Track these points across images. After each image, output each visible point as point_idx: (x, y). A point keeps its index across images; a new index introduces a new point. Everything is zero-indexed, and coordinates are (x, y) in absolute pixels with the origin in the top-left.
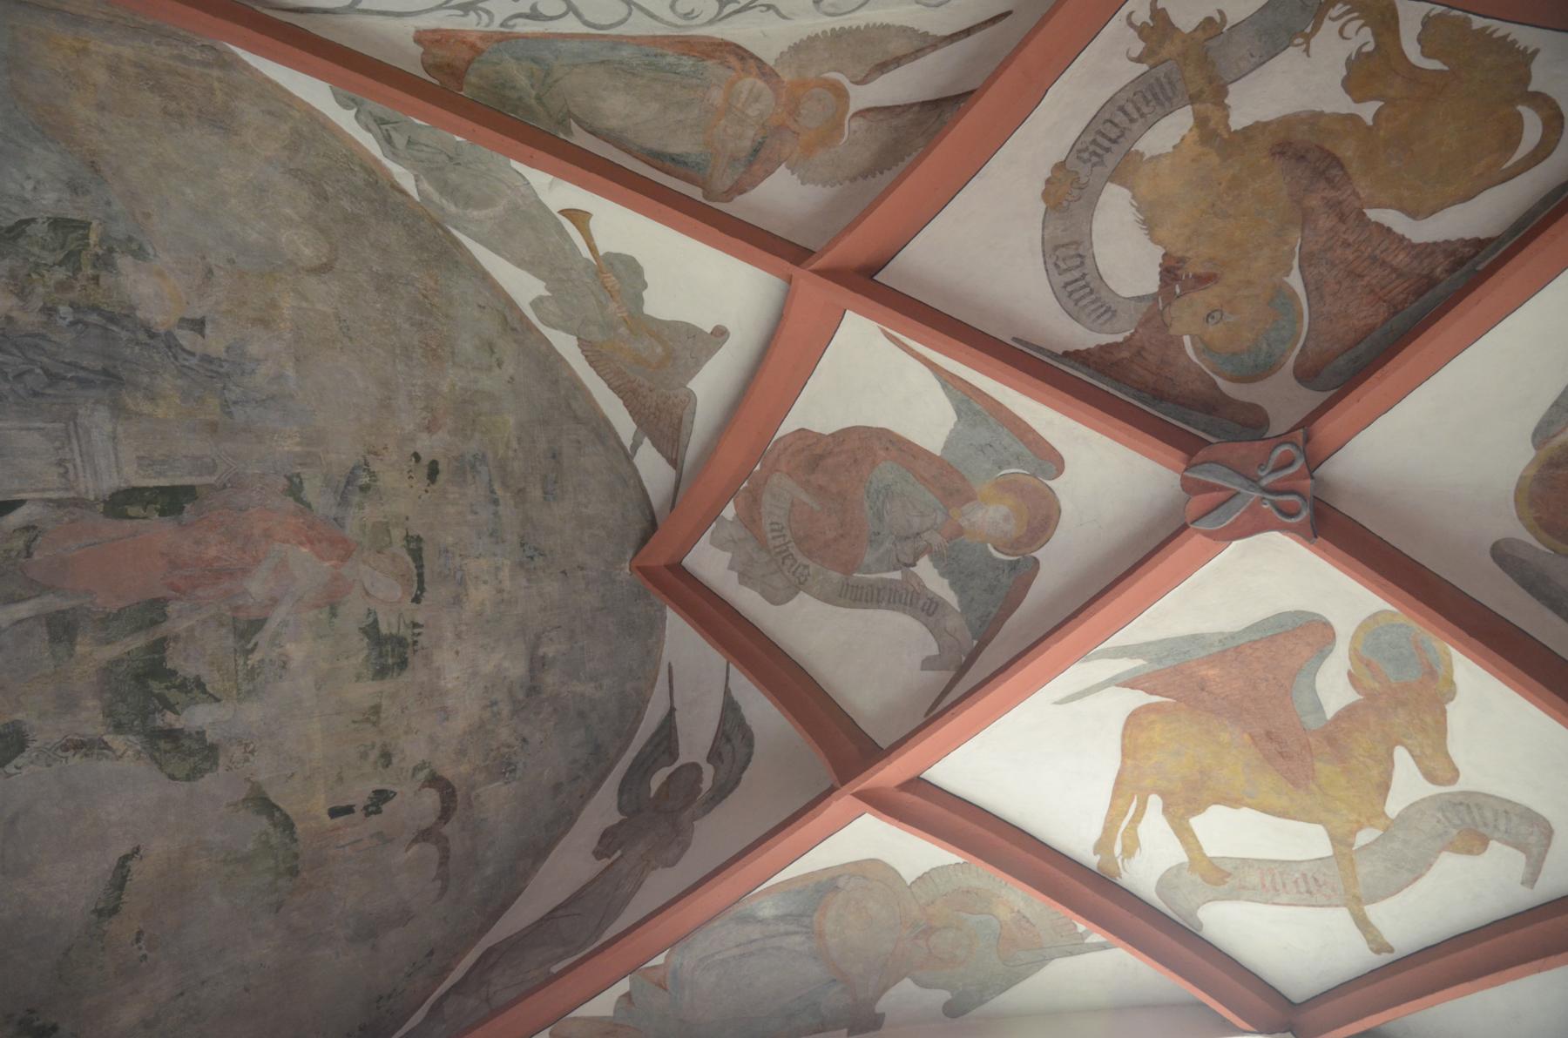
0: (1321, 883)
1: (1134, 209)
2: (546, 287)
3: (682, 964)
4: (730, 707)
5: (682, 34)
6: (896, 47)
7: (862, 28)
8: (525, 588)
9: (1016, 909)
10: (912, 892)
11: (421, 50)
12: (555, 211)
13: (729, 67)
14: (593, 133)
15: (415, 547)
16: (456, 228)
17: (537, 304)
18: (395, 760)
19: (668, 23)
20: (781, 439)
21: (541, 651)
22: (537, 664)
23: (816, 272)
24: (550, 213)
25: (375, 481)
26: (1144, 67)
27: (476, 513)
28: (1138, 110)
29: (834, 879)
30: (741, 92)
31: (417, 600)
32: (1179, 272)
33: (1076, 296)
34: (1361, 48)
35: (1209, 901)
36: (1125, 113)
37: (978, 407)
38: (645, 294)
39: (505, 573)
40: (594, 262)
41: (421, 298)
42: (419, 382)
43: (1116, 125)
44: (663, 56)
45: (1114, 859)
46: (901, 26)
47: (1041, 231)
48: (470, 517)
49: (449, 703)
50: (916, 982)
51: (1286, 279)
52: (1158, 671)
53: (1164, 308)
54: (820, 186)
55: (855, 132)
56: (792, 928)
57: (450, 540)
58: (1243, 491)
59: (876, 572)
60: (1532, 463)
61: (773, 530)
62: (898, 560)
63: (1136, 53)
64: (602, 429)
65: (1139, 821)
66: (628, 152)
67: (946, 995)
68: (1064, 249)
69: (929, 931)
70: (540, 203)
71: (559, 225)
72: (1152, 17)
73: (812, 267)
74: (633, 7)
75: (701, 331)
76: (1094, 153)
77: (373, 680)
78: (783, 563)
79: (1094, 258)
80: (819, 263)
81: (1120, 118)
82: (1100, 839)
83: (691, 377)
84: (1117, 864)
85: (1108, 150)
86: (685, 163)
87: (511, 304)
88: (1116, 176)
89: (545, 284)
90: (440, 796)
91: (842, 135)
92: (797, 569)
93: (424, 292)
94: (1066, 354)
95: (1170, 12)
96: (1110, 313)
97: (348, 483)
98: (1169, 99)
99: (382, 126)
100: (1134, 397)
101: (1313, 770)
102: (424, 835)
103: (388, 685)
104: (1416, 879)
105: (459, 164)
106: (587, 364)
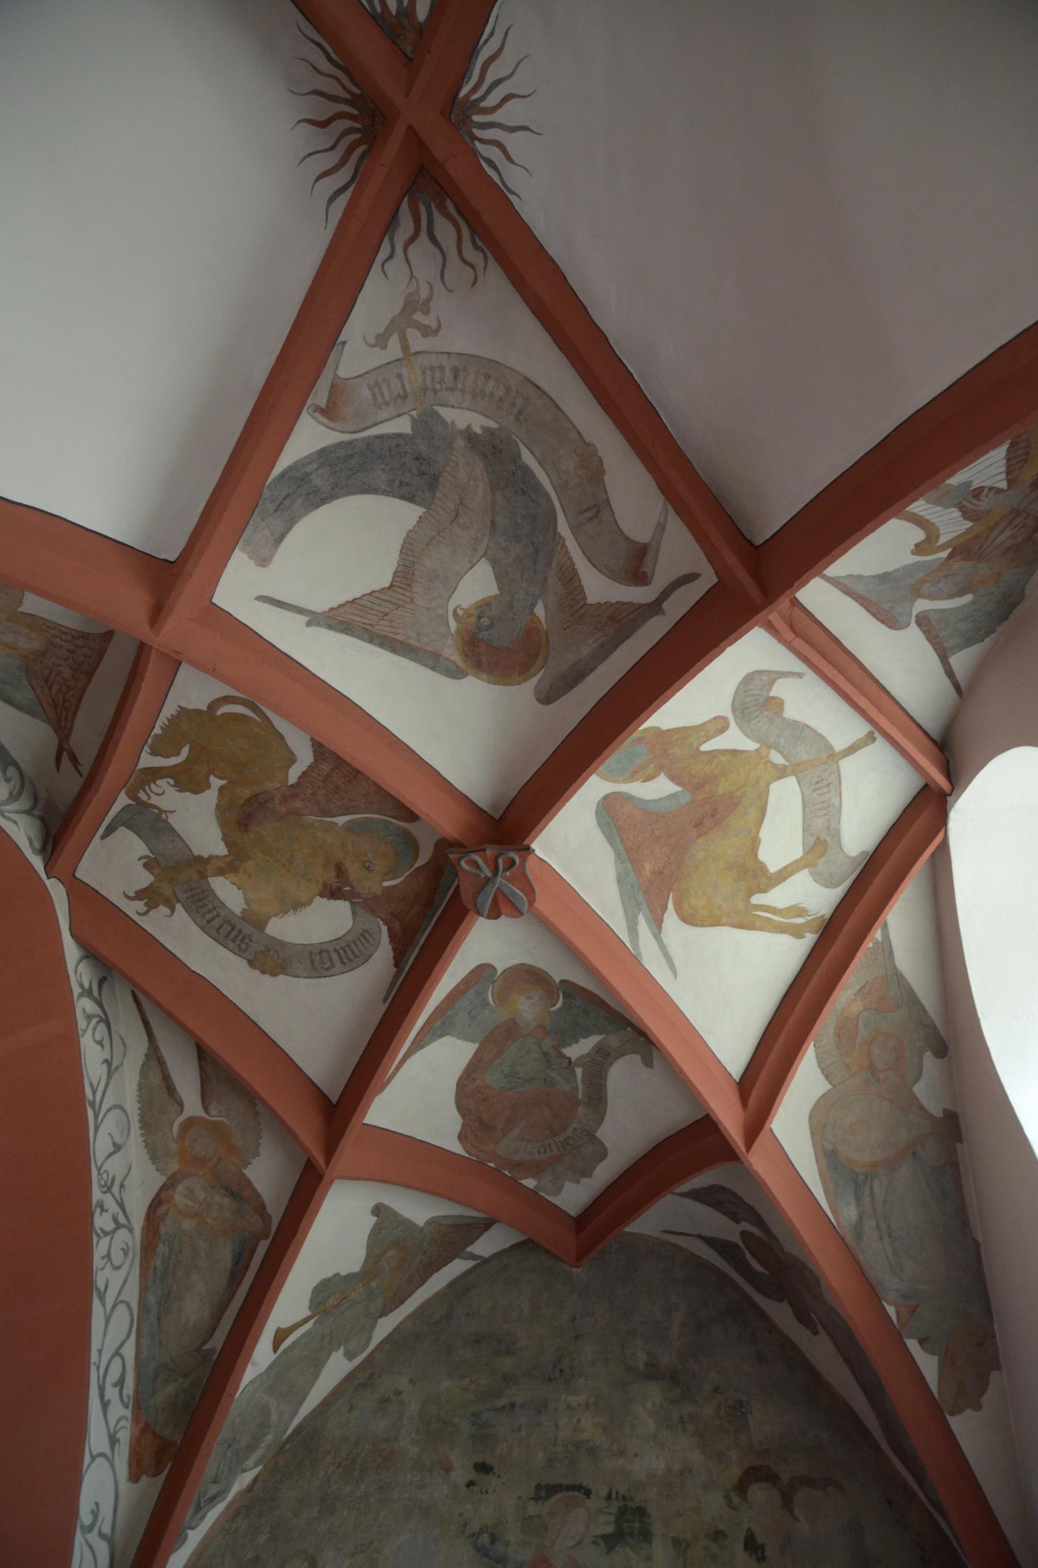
0: (820, 779)
1: (285, 916)
2: (336, 1351)
3: (897, 1291)
4: (694, 1195)
5: (139, 1252)
6: (156, 1078)
7: (140, 1106)
8: (586, 1380)
9: (853, 997)
10: (839, 1084)
11: (144, 1478)
12: (275, 1356)
13: (166, 1214)
14: (214, 1329)
15: (545, 1491)
16: (285, 1431)
17: (350, 1356)
18: (721, 1527)
19: (131, 1268)
20: (467, 1152)
21: (641, 1366)
22: (652, 1373)
23: (328, 1161)
24: (275, 1361)
25: (487, 1527)
26: (179, 907)
27: (520, 1426)
28: (210, 911)
29: (826, 1153)
30: (186, 1205)
31: (588, 1493)
32: (334, 888)
33: (351, 956)
34: (173, 786)
35: (841, 849)
36: (213, 919)
37: (439, 1022)
38: (344, 1273)
39: (574, 1400)
40: (317, 1317)
41: (340, 1470)
42: (409, 1476)
43: (221, 926)
44: (155, 1269)
45: (808, 922)
46: (140, 1075)
47: (300, 979)
48: (523, 1433)
49: (677, 1467)
50: (917, 1080)
51: (342, 1350)
52: (647, 904)
53: (361, 898)
54: (261, 1141)
55: (220, 1112)
56: (867, 1192)
57: (540, 1455)
58: (496, 886)
59: (577, 1084)
60: (476, 676)
61: (545, 1152)
62: (567, 1068)
63: (168, 912)
64: (458, 1288)
65: (775, 908)
66: (229, 1300)
67: (928, 1058)
68: (316, 963)
69: (872, 1069)
70: (267, 1370)
71: (285, 1351)
72: (142, 900)
73: (323, 1166)
74: (118, 1301)
75: (376, 1224)
76: (242, 940)
77: (651, 1543)
78: (572, 1145)
79: (322, 943)
80: (320, 1159)
81: (216, 923)
82: (791, 934)
83: (415, 1224)
84: (812, 920)
85: (240, 932)
86: (240, 1253)
87: (350, 1377)
88: (261, 926)
89: (334, 1353)
90: (756, 1482)
91: (221, 1122)
92: (577, 1136)
93: (336, 1466)
94: (397, 965)
95: (137, 889)
96: (366, 935)
97: (487, 1555)
98: (203, 891)
99: (202, 1506)
100: (430, 921)
101: (725, 794)
102: (787, 1502)
103: (657, 1528)
104: (809, 727)
105: (234, 1439)
106: (402, 1306)
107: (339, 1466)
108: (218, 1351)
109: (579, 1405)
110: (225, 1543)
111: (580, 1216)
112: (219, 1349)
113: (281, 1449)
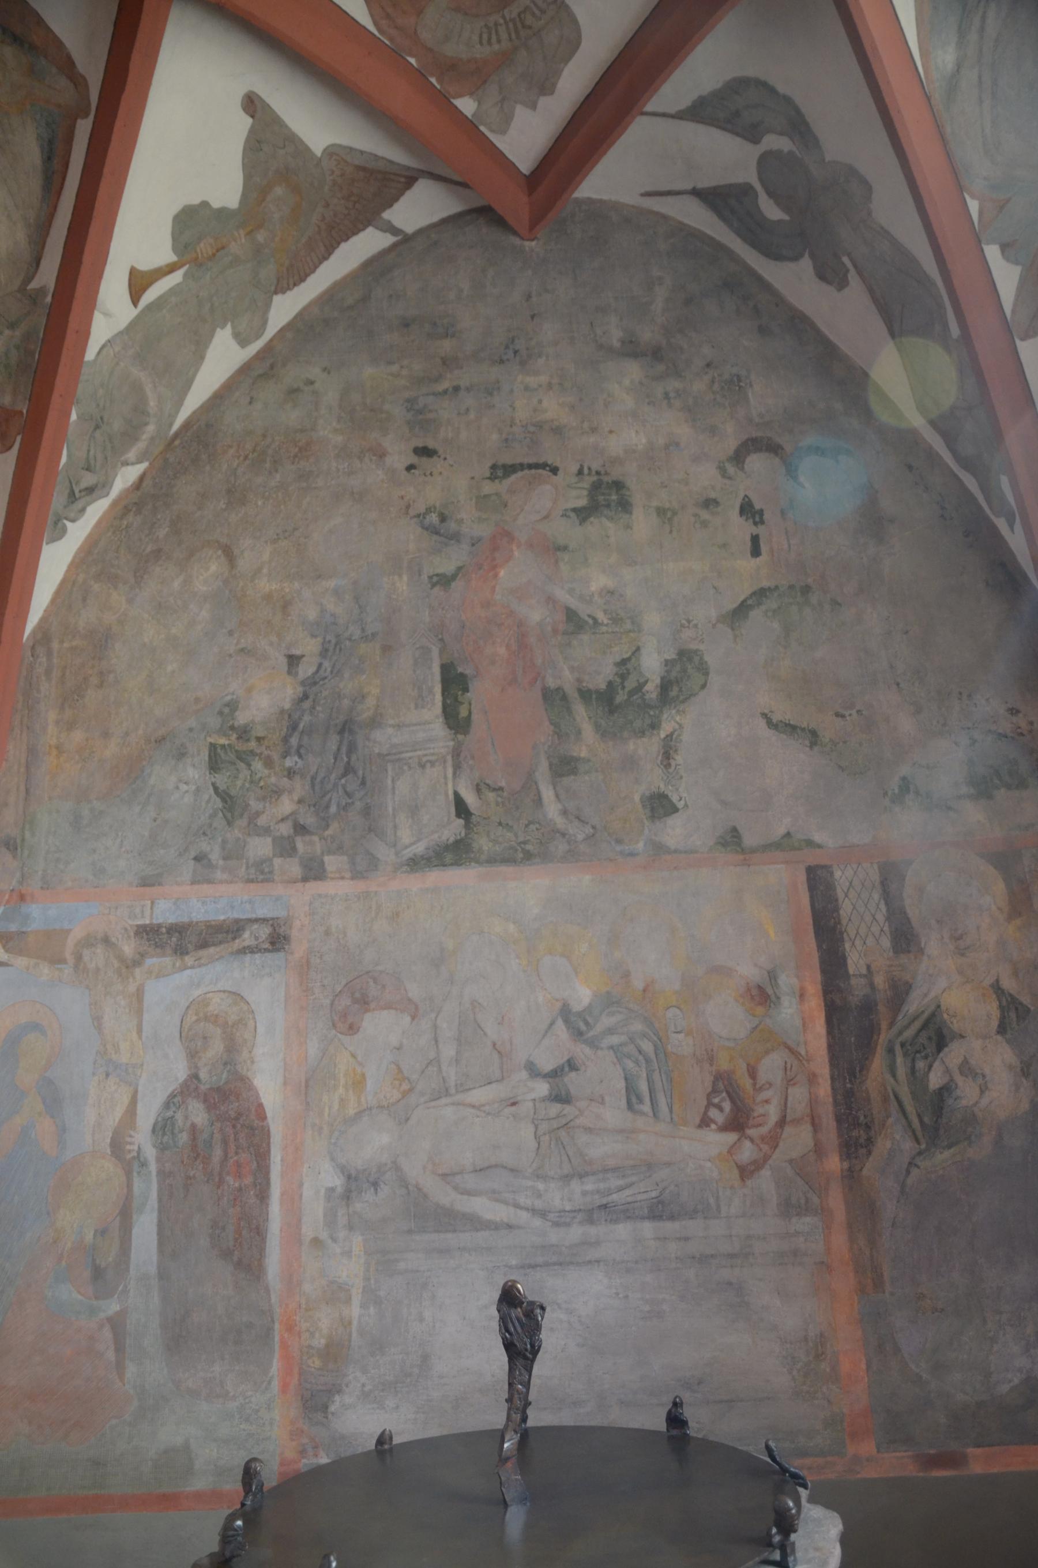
3: (985, 178)
17: (243, 341)
18: (713, 495)
21: (616, 344)
22: (631, 349)
25: (435, 508)
27: (468, 410)
31: (555, 470)
38: (216, 204)
39: (532, 381)
41: (247, 462)
42: (334, 464)
48: (472, 416)
49: (661, 441)
77: (631, 513)
86: (51, 142)
87: (245, 369)
89: (218, 329)
90: (755, 453)
93: (242, 458)
103: (637, 499)
107: (246, 458)
108: (52, 290)
109: (540, 386)
110: (116, 539)
111: (533, 173)
112: (51, 286)
113: (170, 445)
